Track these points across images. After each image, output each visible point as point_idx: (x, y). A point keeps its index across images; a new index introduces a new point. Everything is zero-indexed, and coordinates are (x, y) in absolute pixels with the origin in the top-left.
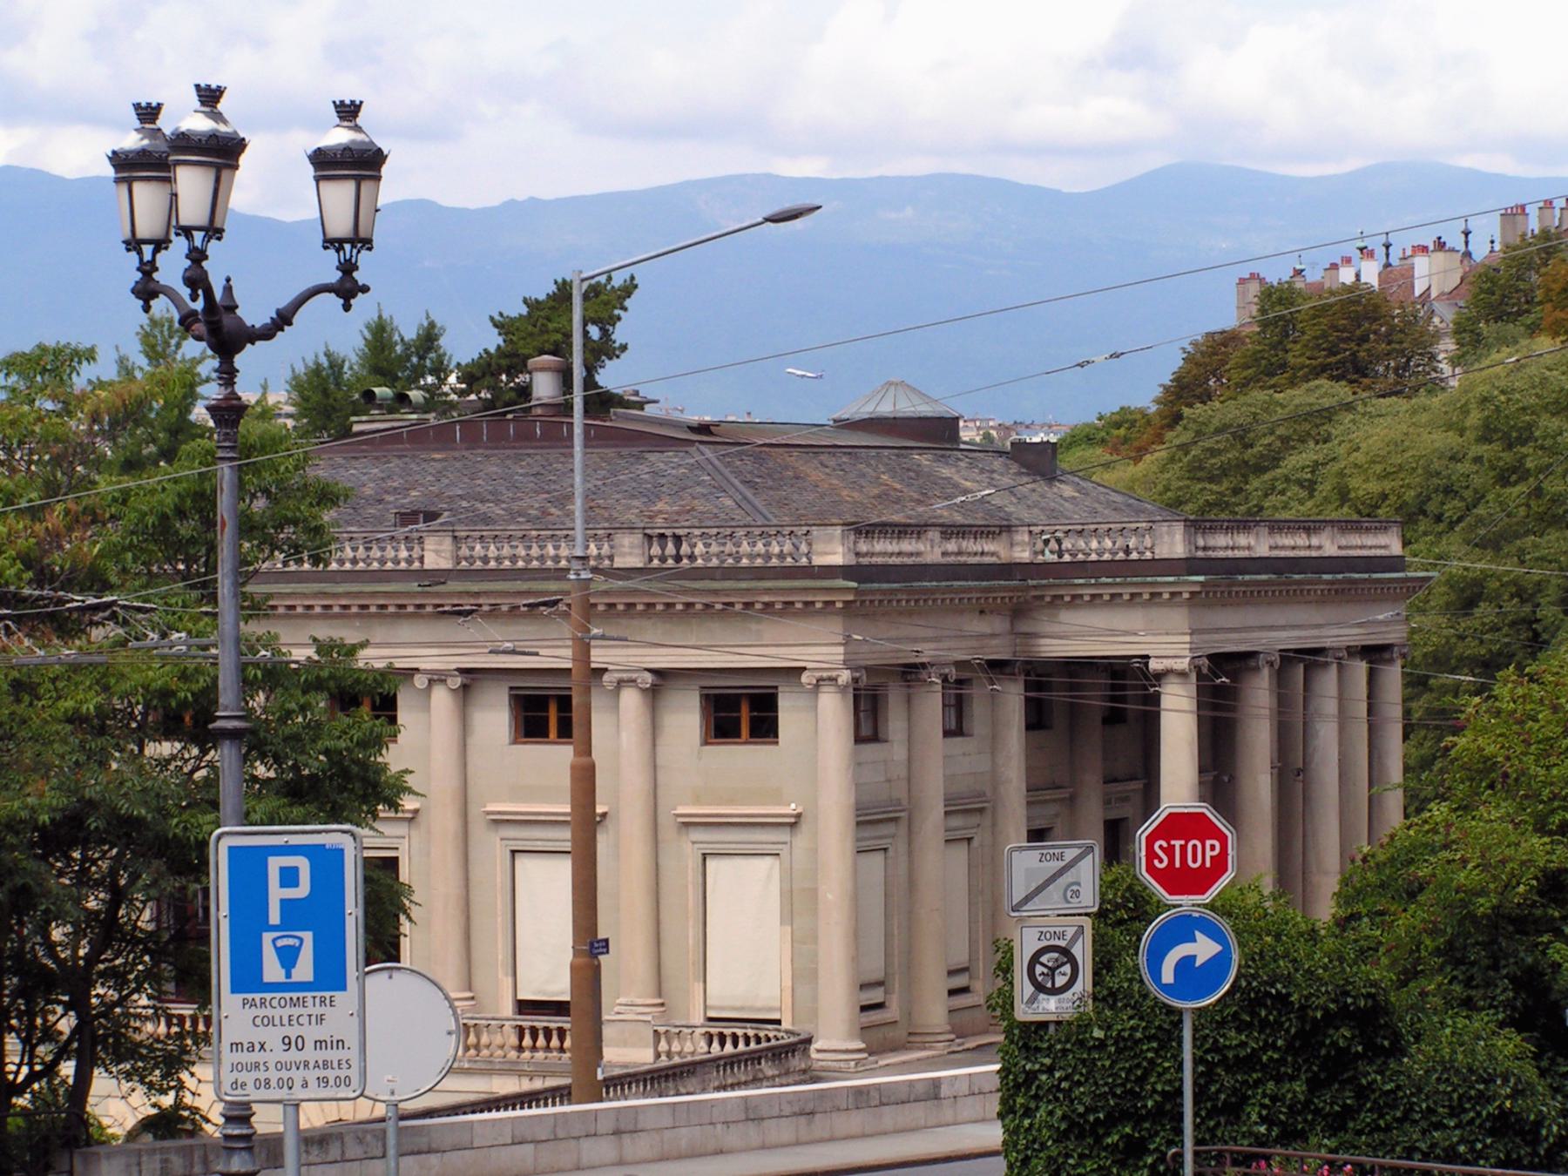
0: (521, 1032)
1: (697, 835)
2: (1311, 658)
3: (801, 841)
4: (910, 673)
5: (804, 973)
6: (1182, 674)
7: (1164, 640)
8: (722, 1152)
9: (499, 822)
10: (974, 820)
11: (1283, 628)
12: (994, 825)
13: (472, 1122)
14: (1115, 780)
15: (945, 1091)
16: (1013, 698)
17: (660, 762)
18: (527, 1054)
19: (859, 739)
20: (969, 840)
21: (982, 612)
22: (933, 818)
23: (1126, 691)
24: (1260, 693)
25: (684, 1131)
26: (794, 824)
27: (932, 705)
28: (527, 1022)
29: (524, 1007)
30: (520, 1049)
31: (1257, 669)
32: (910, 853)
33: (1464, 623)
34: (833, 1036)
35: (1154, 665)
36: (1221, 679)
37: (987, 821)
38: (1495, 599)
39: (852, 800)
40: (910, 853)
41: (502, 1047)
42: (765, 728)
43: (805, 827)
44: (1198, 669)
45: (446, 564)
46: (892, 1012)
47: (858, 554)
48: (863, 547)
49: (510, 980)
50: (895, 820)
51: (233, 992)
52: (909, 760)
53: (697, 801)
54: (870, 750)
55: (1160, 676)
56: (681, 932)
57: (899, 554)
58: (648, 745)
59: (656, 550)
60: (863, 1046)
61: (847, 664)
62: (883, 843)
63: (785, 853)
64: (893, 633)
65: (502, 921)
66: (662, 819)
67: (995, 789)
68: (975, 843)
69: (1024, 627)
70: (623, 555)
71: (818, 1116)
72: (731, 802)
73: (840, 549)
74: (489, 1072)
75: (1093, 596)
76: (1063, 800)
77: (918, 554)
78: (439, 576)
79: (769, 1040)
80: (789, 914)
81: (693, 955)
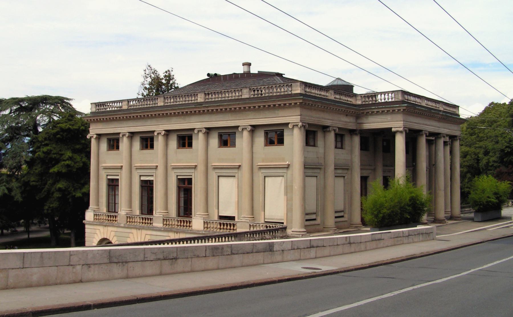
0: (220, 224)
1: (263, 171)
2: (437, 135)
3: (289, 172)
4: (325, 128)
5: (289, 210)
6: (401, 132)
7: (396, 123)
8: (81, 281)
9: (215, 168)
10: (346, 171)
11: (429, 125)
12: (351, 173)
13: (273, 243)
14: (387, 166)
15: (276, 248)
16: (357, 140)
17: (254, 151)
18: (222, 230)
19: (307, 144)
20: (344, 177)
21: (347, 115)
22: (331, 169)
23: (387, 136)
24: (422, 142)
25: (35, 270)
26: (288, 167)
27: (331, 137)
28: (222, 221)
29: (221, 217)
30: (220, 229)
31: (422, 135)
32: (325, 178)
33: (465, 159)
34: (296, 226)
35: (393, 130)
36: (412, 137)
37: (349, 172)
38: (470, 155)
39: (303, 160)
40: (325, 178)
41: (213, 228)
42: (281, 142)
43: (290, 168)
44: (406, 131)
45: (202, 101)
46: (318, 221)
47: (305, 91)
48: (308, 90)
49: (217, 210)
50: (320, 168)
51: (234, 217)
52: (325, 153)
53: (263, 162)
54: (310, 148)
55: (395, 132)
56: (258, 197)
57: (320, 95)
58: (250, 146)
59: (252, 93)
60: (305, 230)
61: (301, 121)
62: (315, 175)
63: (285, 176)
64: (318, 116)
65: (215, 194)
66: (254, 167)
67: (352, 164)
68: (346, 177)
69: (359, 121)
70: (244, 95)
71: (179, 261)
72: (272, 162)
73: (299, 89)
74: (170, 231)
75: (377, 112)
76: (372, 169)
77: (327, 96)
78: (201, 104)
79: (270, 227)
80: (286, 193)
81: (261, 204)
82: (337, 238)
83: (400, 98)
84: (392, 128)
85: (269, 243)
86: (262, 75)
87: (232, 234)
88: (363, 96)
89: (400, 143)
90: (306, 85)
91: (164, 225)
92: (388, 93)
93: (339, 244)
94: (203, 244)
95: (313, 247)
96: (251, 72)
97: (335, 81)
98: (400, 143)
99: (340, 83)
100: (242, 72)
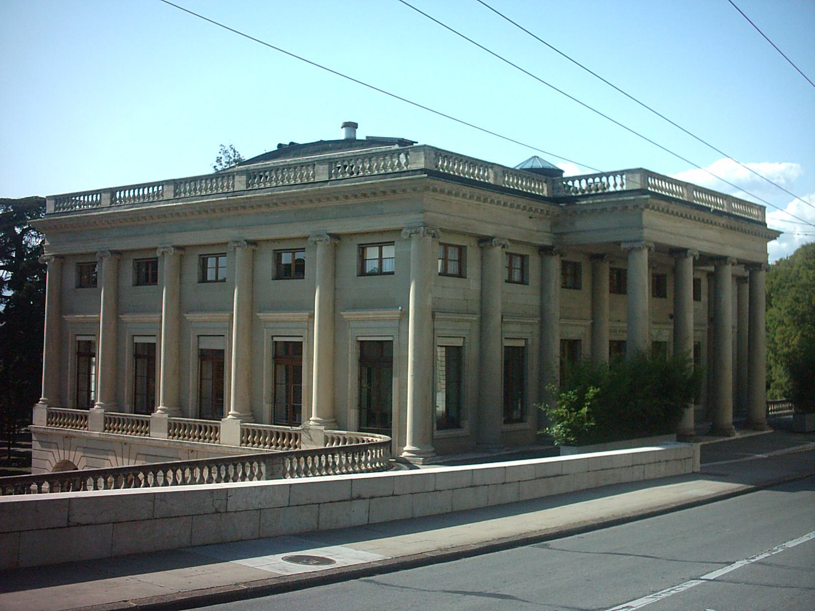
83: (636, 183)
86: (371, 141)
87: (292, 453)
90: (439, 153)
91: (170, 435)
92: (614, 174)
94: (102, 493)
96: (357, 138)
99: (538, 165)
100: (768, 252)
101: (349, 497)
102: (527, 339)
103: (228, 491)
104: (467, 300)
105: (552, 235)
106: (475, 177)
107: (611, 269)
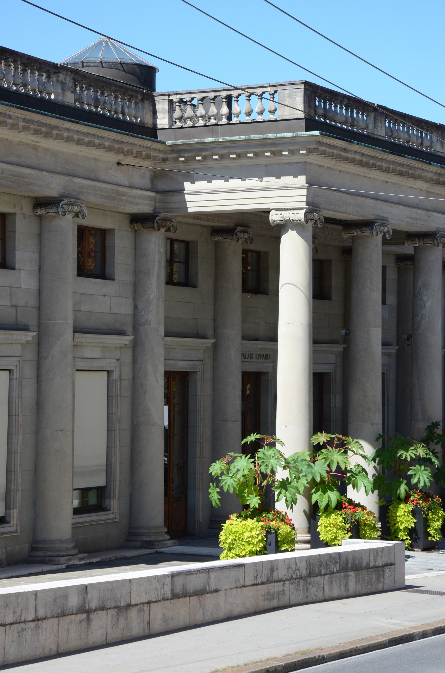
7: (283, 196)
23: (254, 235)
24: (372, 256)
35: (274, 217)
55: (282, 227)
82: (36, 593)
84: (267, 212)
85: (271, 562)
88: (176, 98)
89: (294, 259)
93: (41, 614)
95: (186, 595)
97: (97, 46)
98: (294, 259)
101: (151, 604)
102: (112, 371)
103: (36, 595)
104: (16, 306)
105: (152, 194)
106: (82, 103)
107: (245, 252)
